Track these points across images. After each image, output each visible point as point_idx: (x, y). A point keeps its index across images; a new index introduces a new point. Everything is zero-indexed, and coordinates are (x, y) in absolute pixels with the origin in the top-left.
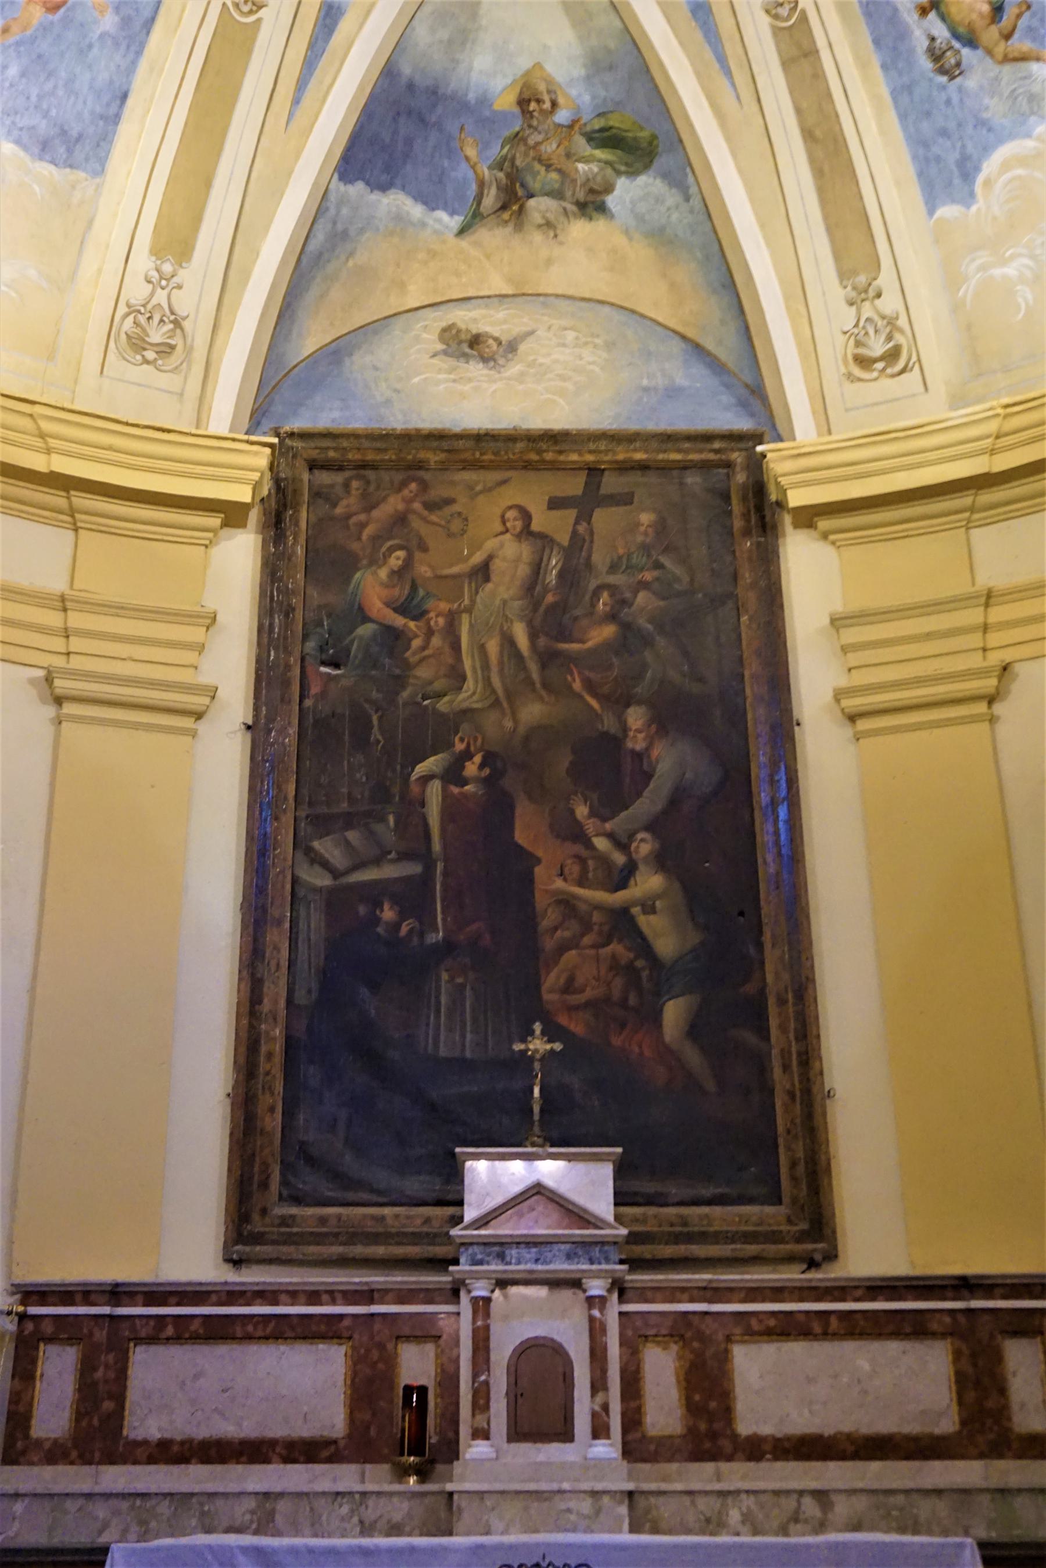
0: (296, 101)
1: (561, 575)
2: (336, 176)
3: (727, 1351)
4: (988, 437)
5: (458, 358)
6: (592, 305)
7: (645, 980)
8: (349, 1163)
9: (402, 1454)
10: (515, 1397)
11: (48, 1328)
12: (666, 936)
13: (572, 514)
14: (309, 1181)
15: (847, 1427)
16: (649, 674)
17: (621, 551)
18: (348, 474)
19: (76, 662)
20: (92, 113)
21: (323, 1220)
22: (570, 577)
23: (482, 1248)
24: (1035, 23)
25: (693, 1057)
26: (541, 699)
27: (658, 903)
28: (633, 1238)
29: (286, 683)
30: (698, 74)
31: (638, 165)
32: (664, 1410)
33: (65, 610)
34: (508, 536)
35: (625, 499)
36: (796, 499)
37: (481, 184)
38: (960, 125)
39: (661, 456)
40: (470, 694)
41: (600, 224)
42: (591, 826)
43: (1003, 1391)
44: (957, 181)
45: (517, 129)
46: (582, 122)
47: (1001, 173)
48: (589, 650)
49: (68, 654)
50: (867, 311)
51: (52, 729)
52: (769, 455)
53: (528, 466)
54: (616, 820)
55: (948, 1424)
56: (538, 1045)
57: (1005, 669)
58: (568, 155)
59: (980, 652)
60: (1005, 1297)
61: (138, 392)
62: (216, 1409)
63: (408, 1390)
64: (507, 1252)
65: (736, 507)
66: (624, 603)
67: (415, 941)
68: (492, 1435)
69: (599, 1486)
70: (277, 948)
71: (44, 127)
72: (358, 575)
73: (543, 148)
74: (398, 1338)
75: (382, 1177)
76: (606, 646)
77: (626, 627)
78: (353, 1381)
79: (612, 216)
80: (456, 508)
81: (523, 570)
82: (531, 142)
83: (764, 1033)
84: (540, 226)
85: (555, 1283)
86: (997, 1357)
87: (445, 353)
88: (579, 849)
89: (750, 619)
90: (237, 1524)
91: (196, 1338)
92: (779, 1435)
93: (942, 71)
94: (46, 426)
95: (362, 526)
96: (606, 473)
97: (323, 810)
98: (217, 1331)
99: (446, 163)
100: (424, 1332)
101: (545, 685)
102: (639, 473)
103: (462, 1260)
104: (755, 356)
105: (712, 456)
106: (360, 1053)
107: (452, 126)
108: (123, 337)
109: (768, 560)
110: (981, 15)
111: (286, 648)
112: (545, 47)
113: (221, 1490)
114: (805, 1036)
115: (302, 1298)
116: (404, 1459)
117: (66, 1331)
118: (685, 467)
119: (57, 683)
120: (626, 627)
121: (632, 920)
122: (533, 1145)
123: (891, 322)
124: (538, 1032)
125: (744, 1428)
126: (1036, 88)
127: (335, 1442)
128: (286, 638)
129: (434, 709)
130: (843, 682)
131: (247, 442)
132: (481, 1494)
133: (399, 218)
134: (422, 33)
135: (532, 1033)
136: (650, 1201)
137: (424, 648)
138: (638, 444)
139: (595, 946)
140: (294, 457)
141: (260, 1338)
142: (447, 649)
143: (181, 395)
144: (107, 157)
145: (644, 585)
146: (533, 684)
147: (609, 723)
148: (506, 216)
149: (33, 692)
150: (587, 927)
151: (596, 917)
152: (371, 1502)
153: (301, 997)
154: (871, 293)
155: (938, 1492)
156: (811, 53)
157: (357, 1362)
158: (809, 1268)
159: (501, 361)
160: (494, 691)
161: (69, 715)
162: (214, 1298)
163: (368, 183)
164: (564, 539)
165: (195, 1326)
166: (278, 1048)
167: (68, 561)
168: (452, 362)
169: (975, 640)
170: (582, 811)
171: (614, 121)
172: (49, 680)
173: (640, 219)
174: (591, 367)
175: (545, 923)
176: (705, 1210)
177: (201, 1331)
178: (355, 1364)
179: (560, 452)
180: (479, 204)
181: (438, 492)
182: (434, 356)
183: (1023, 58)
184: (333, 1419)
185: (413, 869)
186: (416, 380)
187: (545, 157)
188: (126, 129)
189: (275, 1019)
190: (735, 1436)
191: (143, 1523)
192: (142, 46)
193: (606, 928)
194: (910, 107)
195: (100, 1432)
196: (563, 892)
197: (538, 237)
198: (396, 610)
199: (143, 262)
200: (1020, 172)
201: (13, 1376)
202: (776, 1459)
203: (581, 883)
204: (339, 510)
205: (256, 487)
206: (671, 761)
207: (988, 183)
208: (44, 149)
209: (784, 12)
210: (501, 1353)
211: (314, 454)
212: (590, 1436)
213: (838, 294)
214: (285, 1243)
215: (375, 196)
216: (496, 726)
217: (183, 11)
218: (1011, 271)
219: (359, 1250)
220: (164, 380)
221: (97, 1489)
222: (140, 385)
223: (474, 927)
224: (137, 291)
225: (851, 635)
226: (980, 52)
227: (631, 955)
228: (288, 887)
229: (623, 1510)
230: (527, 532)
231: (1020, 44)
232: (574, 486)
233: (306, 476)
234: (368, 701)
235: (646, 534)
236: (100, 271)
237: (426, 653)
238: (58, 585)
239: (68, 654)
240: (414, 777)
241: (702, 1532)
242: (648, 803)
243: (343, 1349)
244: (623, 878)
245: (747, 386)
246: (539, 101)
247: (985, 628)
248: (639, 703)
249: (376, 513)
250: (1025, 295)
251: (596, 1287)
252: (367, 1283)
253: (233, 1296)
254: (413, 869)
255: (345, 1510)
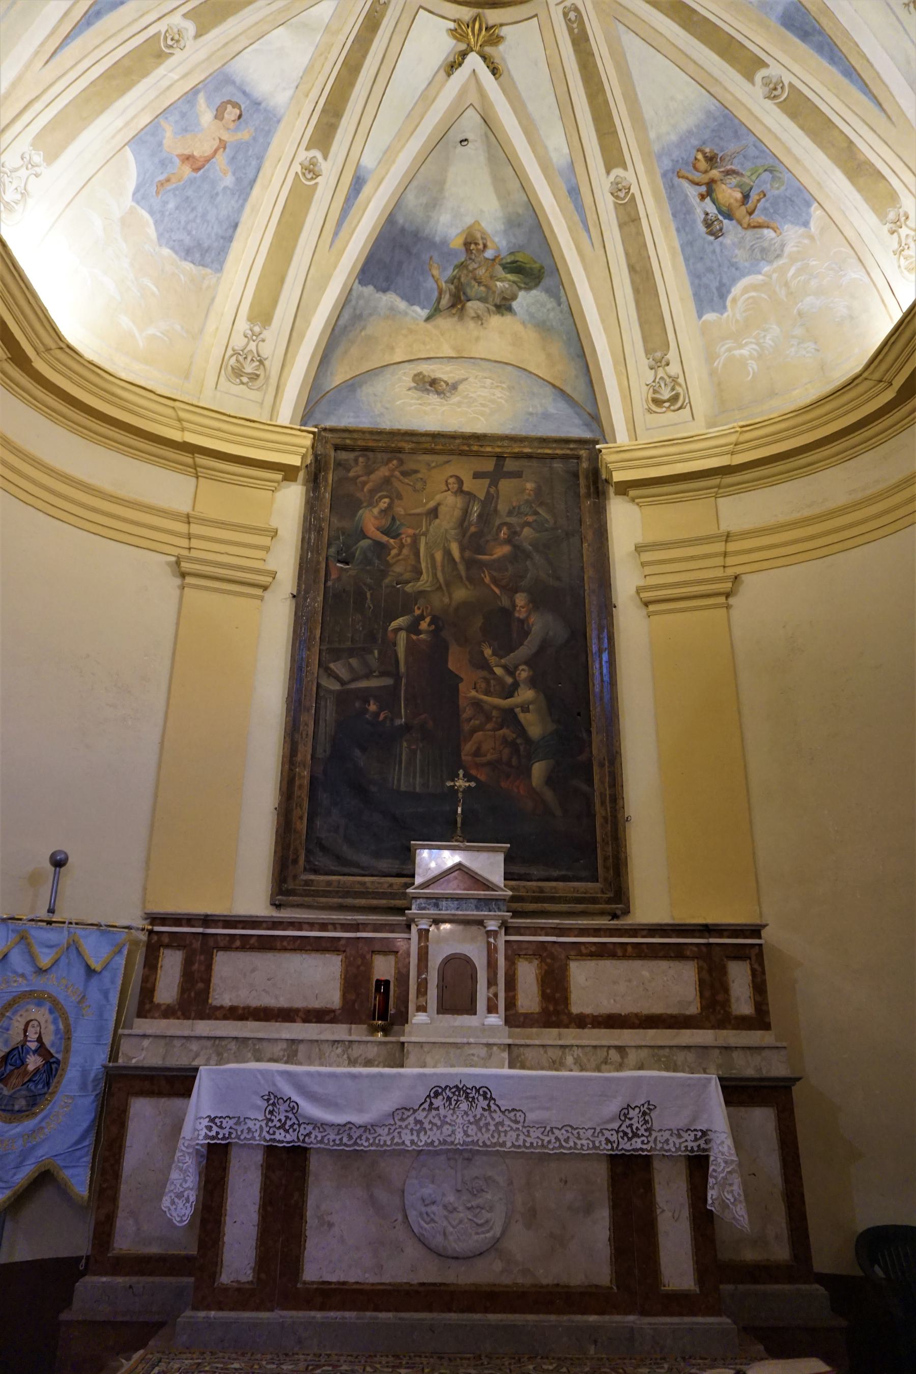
0: (336, 234)
1: (480, 516)
2: (357, 281)
3: (567, 965)
4: (730, 444)
5: (423, 391)
6: (501, 365)
7: (521, 750)
8: (347, 851)
9: (374, 1019)
10: (442, 987)
11: (166, 940)
12: (535, 725)
13: (487, 482)
14: (322, 860)
15: (635, 1010)
16: (529, 576)
17: (514, 504)
18: (357, 454)
19: (194, 554)
20: (217, 234)
21: (329, 883)
22: (484, 517)
23: (425, 900)
24: (768, 205)
25: (549, 795)
26: (467, 588)
27: (531, 707)
28: (513, 899)
29: (317, 571)
30: (569, 228)
31: (533, 284)
32: (529, 998)
33: (189, 523)
34: (449, 492)
35: (518, 475)
36: (617, 477)
37: (441, 292)
38: (720, 266)
39: (539, 451)
40: (425, 582)
41: (508, 319)
42: (493, 660)
43: (726, 990)
44: (716, 299)
45: (463, 260)
46: (502, 256)
47: (742, 295)
48: (494, 561)
49: (190, 549)
50: (661, 373)
51: (178, 592)
52: (603, 451)
53: (462, 453)
54: (507, 658)
55: (694, 1009)
56: (461, 783)
57: (736, 578)
58: (492, 277)
59: (722, 568)
60: (729, 937)
61: (237, 399)
62: (264, 990)
63: (379, 982)
64: (440, 903)
65: (582, 481)
66: (515, 533)
67: (388, 724)
68: (428, 1010)
69: (491, 1041)
70: (306, 725)
71: (187, 240)
72: (361, 512)
73: (477, 272)
74: (373, 952)
75: (364, 859)
76: (504, 557)
77: (517, 548)
78: (345, 976)
79: (515, 314)
80: (419, 475)
81: (458, 513)
82: (470, 268)
83: (590, 781)
84: (473, 318)
85: (466, 922)
86: (724, 971)
87: (415, 388)
88: (485, 673)
89: (589, 545)
90: (275, 1057)
91: (253, 949)
92: (595, 1014)
93: (711, 233)
94: (182, 415)
95: (364, 484)
96: (507, 459)
97: (336, 645)
98: (266, 945)
99: (421, 279)
100: (388, 950)
101: (468, 578)
102: (526, 460)
103: (413, 907)
104: (596, 399)
105: (568, 452)
106: (349, 794)
107: (425, 257)
108: (230, 368)
109: (600, 512)
110: (736, 200)
111: (317, 551)
112: (482, 211)
113: (266, 1037)
114: (614, 785)
115: (317, 926)
116: (375, 1022)
117: (176, 942)
118: (553, 457)
119: (183, 564)
120: (517, 548)
121: (515, 716)
122: (457, 841)
123: (674, 380)
124: (461, 776)
125: (575, 1009)
126: (766, 244)
127: (334, 1011)
128: (318, 546)
129: (403, 590)
130: (642, 583)
131: (299, 430)
132: (421, 1044)
133: (392, 309)
134: (411, 199)
135: (458, 776)
136: (520, 878)
137: (399, 555)
138: (526, 443)
139: (494, 730)
140: (326, 442)
141: (291, 950)
142: (412, 557)
143: (262, 403)
144: (224, 262)
145: (528, 524)
146: (461, 578)
147: (505, 602)
148: (454, 311)
149: (168, 570)
150: (489, 718)
151: (495, 713)
152: (355, 1046)
153: (320, 754)
154: (664, 363)
155: (688, 1048)
156: (636, 220)
157: (348, 965)
158: (612, 919)
159: (448, 394)
160: (438, 580)
161: (189, 584)
162: (264, 925)
163: (375, 287)
164: (482, 496)
165: (252, 941)
166: (306, 782)
167: (192, 495)
168: (420, 394)
169: (719, 561)
170: (488, 652)
171: (519, 257)
172: (178, 563)
173: (532, 316)
174: (500, 400)
175: (465, 716)
176: (554, 884)
177: (256, 944)
178: (347, 966)
179: (481, 446)
180: (439, 303)
181: (410, 465)
182: (409, 389)
183: (759, 226)
184: (333, 998)
185: (388, 681)
186: (398, 403)
187: (478, 277)
188: (236, 245)
189: (304, 766)
190: (570, 1014)
191: (219, 1054)
192: (248, 195)
193: (500, 720)
194: (692, 256)
195: (195, 1001)
196: (474, 698)
197: (471, 324)
198: (382, 532)
199: (242, 325)
200: (753, 294)
201: (144, 967)
202: (593, 1027)
203: (487, 693)
204: (351, 474)
205: (304, 457)
206: (541, 625)
207: (734, 300)
208: (187, 253)
209: (622, 194)
210: (436, 960)
211: (338, 441)
212: (486, 1011)
213: (644, 362)
214: (306, 896)
215: (379, 295)
216: (438, 601)
217: (272, 175)
218: (745, 352)
219: (350, 901)
220: (255, 395)
221: (193, 1034)
222: (237, 396)
223: (423, 716)
224: (238, 342)
225: (647, 557)
226: (734, 222)
227: (514, 736)
228: (315, 689)
229: (505, 1055)
230: (460, 491)
231: (758, 217)
232: (489, 465)
233: (332, 453)
234: (365, 584)
235: (529, 495)
236: (217, 328)
237: (400, 557)
238: (185, 507)
239: (190, 549)
240: (390, 628)
241: (550, 1069)
242: (526, 650)
243: (340, 958)
244: (510, 691)
245: (589, 414)
246: (476, 244)
247: (725, 554)
248: (523, 592)
249: (373, 477)
250: (753, 365)
251: (492, 925)
252: (355, 920)
253: (276, 924)
254: (388, 681)
255: (339, 1051)
